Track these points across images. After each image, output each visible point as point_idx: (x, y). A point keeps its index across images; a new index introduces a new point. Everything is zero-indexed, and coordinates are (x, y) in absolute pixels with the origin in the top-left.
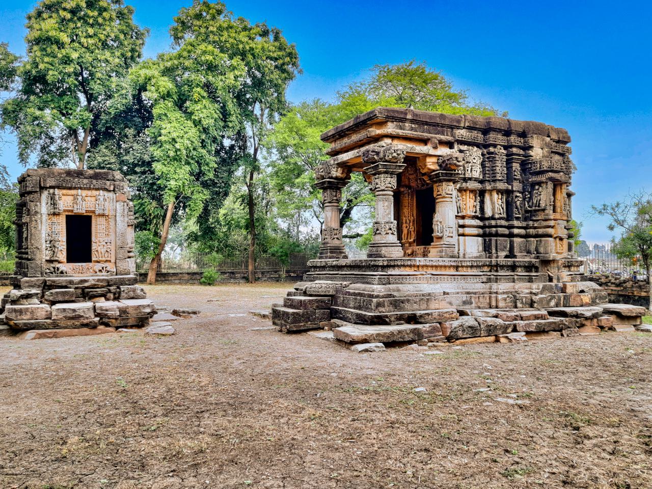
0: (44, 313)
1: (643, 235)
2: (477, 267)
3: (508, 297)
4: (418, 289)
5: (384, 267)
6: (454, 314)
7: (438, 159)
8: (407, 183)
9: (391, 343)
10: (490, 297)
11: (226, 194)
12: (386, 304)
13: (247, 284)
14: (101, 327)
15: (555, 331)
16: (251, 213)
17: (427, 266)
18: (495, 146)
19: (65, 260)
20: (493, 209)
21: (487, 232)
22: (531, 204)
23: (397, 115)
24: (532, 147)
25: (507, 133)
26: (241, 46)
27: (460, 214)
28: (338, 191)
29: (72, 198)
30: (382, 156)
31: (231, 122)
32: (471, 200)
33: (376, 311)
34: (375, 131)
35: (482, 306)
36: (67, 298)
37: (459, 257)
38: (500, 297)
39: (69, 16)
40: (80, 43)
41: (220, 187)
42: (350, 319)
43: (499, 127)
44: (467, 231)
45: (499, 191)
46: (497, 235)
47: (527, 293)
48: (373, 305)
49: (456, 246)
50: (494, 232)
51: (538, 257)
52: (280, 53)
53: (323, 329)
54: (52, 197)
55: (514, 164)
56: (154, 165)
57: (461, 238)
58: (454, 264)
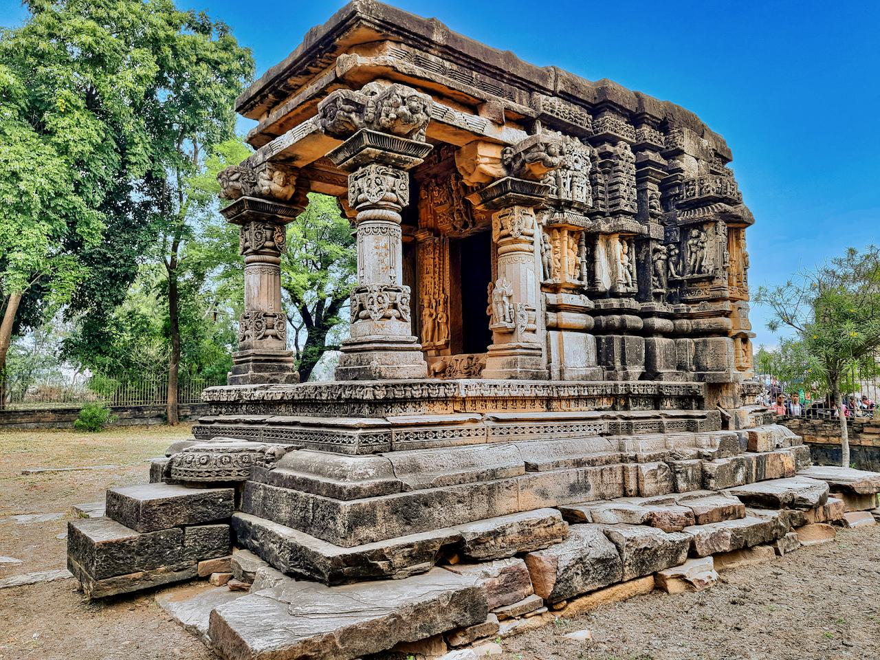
1: (252, 398)
2: (590, 399)
3: (659, 467)
5: (375, 404)
6: (558, 526)
7: (504, 153)
8: (431, 222)
10: (624, 469)
11: (130, 278)
12: (379, 515)
13: (163, 428)
15: (762, 544)
17: (483, 399)
20: (614, 274)
21: (603, 324)
22: (680, 268)
23: (407, 26)
27: (549, 281)
28: (278, 229)
30: (371, 116)
31: (134, 155)
32: (570, 251)
33: (350, 541)
37: (550, 378)
38: (646, 468)
41: (115, 266)
42: (277, 559)
43: (620, 103)
44: (567, 318)
45: (626, 237)
46: (623, 329)
47: (693, 457)
48: (339, 521)
49: (544, 352)
50: (617, 324)
51: (700, 378)
52: (223, 55)
53: (206, 578)
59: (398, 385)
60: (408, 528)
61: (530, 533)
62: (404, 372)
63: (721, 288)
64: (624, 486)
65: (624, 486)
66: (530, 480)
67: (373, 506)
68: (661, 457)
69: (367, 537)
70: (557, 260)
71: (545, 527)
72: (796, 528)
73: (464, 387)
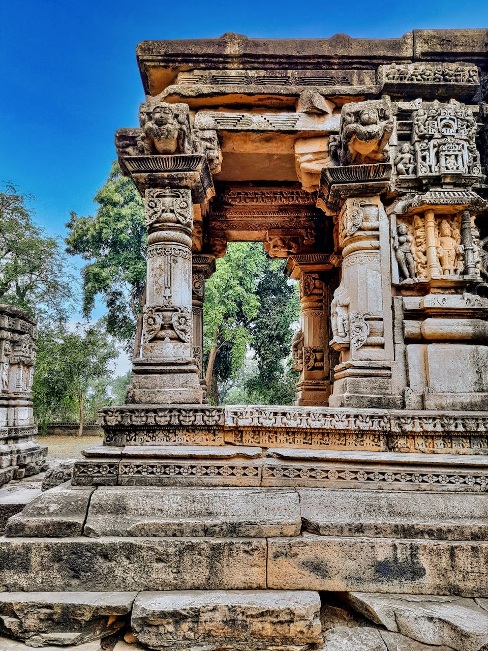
12: (35, 560)
23: (193, 50)
27: (408, 281)
35: (470, 584)
37: (404, 407)
41: (271, 329)
57: (414, 350)
59: (137, 410)
60: (75, 582)
61: (245, 627)
62: (167, 397)
66: (290, 546)
67: (27, 549)
69: (15, 584)
70: (421, 254)
71: (273, 623)
73: (230, 414)
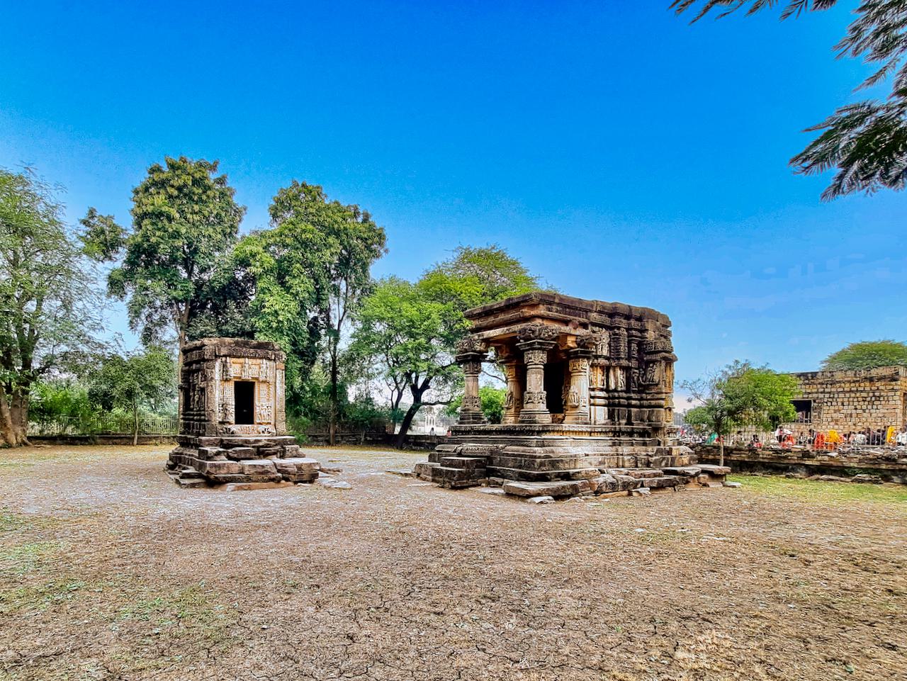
0: (237, 468)
4: (566, 451)
5: (539, 433)
9: (559, 496)
14: (283, 481)
15: (670, 486)
16: (334, 379)
18: (619, 328)
19: (234, 422)
20: (616, 383)
22: (644, 379)
24: (648, 330)
25: (628, 317)
26: (336, 226)
27: (592, 387)
29: (240, 366)
31: (324, 295)
34: (527, 312)
36: (248, 456)
38: (626, 458)
39: (176, 193)
40: (186, 219)
44: (598, 401)
45: (622, 368)
46: (619, 405)
48: (536, 464)
51: (649, 425)
54: (224, 365)
55: (633, 344)
56: (257, 335)
57: (592, 407)
58: (589, 430)
63: (660, 389)
64: (617, 464)
65: (617, 464)
68: (632, 454)
72: (685, 484)
